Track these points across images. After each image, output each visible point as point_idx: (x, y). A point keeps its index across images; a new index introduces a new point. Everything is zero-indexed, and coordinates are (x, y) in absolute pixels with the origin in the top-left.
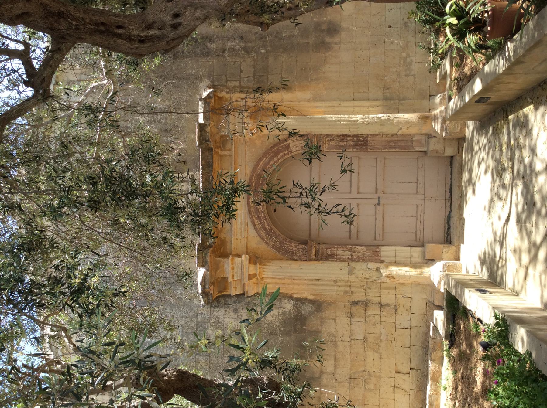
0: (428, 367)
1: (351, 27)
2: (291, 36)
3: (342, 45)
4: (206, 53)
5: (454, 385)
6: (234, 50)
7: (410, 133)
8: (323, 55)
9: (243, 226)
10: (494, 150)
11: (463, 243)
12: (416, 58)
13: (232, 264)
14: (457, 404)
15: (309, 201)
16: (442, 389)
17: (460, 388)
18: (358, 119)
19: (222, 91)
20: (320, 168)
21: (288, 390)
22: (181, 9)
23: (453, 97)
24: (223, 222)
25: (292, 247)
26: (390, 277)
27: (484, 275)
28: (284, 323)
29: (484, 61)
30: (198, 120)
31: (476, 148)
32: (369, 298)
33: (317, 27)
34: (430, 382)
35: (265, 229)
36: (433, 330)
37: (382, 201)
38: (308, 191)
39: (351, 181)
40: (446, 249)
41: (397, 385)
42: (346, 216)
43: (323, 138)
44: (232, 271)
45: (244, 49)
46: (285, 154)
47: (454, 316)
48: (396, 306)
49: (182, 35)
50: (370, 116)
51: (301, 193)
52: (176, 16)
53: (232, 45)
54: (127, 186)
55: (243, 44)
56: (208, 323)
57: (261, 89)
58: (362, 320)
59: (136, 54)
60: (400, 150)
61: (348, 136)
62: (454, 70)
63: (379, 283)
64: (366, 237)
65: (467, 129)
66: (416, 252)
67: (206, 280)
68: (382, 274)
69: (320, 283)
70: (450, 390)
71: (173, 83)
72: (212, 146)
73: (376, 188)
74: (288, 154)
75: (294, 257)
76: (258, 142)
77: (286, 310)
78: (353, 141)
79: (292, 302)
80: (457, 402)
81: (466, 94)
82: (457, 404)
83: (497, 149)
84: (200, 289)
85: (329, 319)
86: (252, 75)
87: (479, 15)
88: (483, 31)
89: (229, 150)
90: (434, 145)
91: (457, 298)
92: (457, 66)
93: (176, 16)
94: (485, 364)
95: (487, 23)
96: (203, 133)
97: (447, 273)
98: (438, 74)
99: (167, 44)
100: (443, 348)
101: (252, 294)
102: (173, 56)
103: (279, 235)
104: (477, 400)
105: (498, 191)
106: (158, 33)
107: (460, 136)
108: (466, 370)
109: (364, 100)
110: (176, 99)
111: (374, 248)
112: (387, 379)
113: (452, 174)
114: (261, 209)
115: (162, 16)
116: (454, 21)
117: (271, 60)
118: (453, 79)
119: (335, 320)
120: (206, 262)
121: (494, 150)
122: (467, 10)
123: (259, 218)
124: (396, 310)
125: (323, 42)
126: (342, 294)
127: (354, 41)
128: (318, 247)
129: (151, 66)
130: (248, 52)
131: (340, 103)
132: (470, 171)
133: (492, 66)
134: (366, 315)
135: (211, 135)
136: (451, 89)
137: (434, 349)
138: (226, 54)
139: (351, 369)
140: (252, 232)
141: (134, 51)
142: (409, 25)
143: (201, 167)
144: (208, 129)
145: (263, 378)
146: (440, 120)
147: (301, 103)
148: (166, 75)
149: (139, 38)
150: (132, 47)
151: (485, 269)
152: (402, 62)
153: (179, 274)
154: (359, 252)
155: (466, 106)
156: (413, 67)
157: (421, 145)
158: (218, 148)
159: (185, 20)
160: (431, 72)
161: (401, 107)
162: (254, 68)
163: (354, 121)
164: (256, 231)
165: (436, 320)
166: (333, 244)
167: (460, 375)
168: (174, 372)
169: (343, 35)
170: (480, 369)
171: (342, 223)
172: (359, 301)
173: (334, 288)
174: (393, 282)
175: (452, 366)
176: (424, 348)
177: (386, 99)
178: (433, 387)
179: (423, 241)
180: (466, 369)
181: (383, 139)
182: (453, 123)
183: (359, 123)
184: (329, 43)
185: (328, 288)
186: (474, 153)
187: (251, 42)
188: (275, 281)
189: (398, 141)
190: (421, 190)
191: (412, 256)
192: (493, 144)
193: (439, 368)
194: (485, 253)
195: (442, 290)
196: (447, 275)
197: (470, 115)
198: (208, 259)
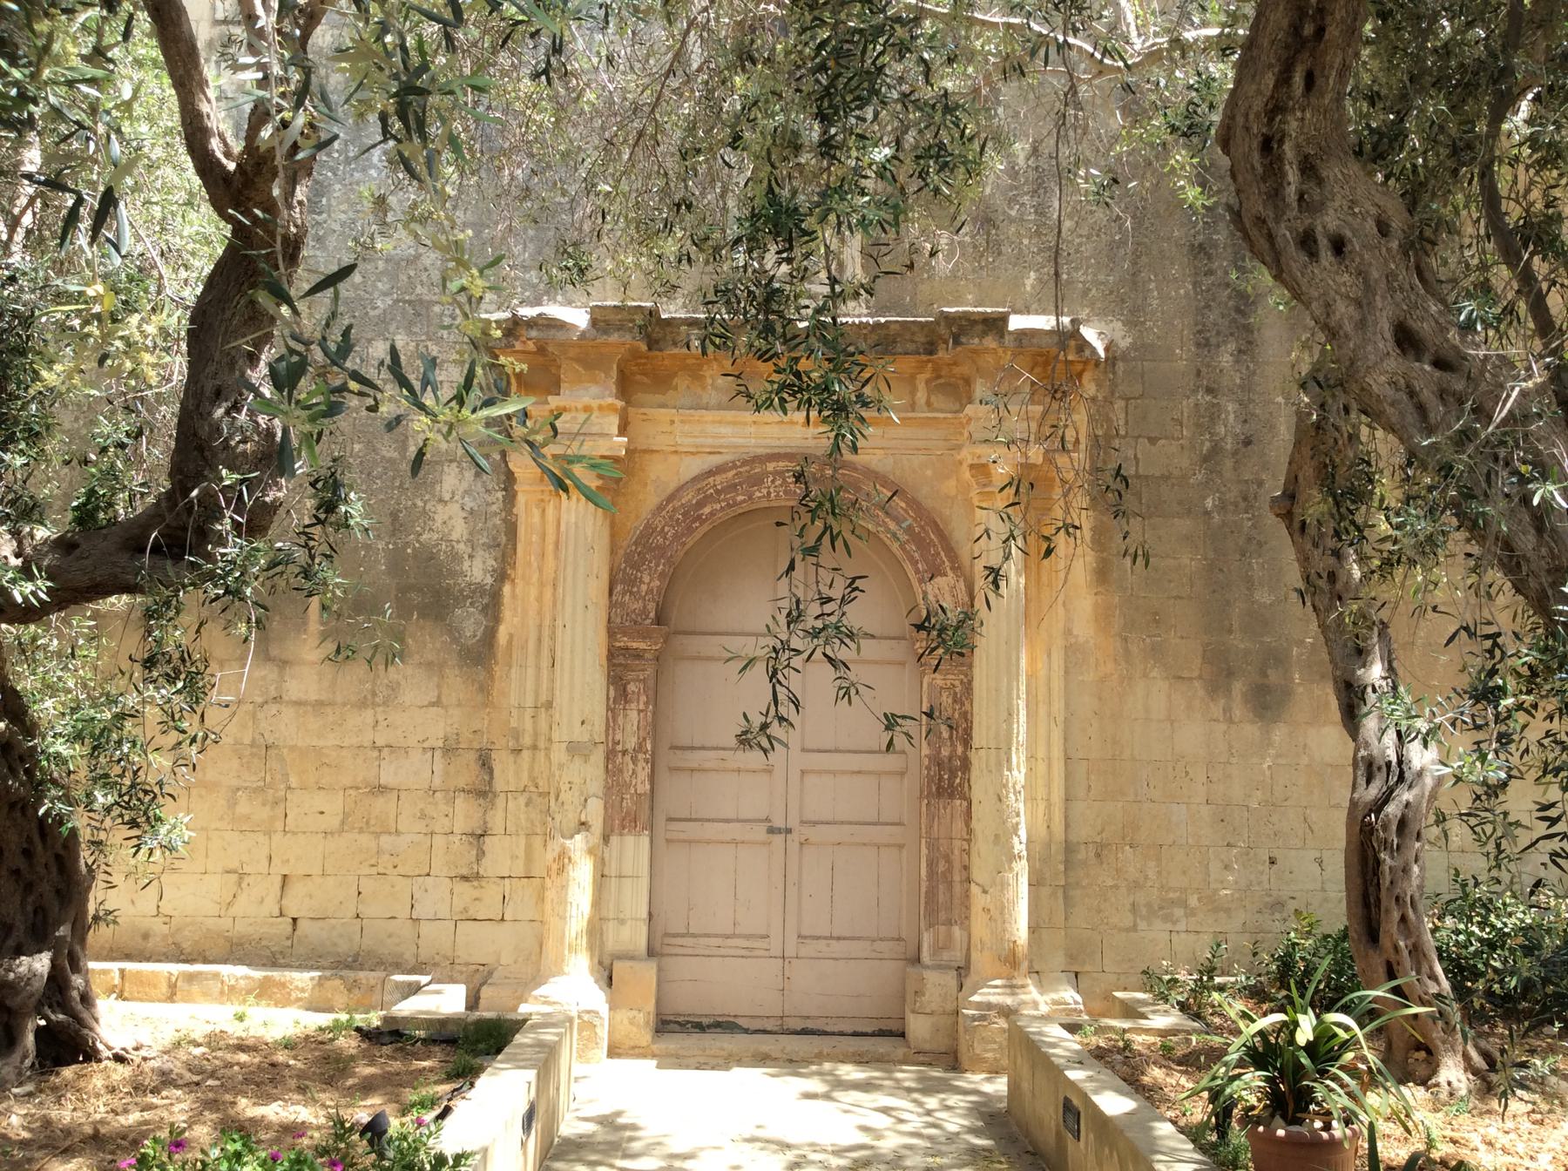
0: (302, 967)
1: (1272, 752)
2: (1250, 583)
3: (1223, 727)
4: (1207, 340)
5: (250, 1042)
6: (1214, 419)
7: (973, 918)
8: (1196, 674)
9: (710, 441)
10: (929, 1153)
11: (658, 1067)
12: (1183, 936)
13: (600, 408)
14: (198, 1051)
15: (810, 622)
16: (240, 1009)
17: (243, 1057)
18: (1015, 773)
19: (1099, 386)
20: (876, 662)
21: (250, 557)
22: (1358, 260)
23: (1077, 1038)
24: (738, 377)
25: (649, 582)
26: (563, 860)
27: (569, 1127)
28: (427, 557)
29: (1182, 1122)
30: (1016, 312)
31: (932, 1102)
32: (500, 801)
33: (1276, 658)
34: (258, 974)
35: (701, 504)
36: (410, 984)
37: (779, 839)
38: (833, 619)
39: (837, 751)
40: (641, 1017)
41: (247, 880)
42: (764, 726)
43: (961, 672)
44: (580, 406)
45: (1216, 450)
46: (914, 563)
47: (451, 1041)
48: (478, 876)
49: (1283, 260)
50: (1021, 806)
51: (830, 600)
52: (1338, 246)
53: (1228, 413)
54: (857, 93)
55: (1229, 445)
56: (427, 334)
57: (1122, 487)
58: (437, 782)
59: (1229, 128)
60: (923, 889)
61: (967, 742)
62: (1151, 1039)
63: (543, 830)
64: (675, 795)
65: (984, 1076)
66: (634, 936)
67: (553, 332)
68: (572, 837)
69: (545, 663)
70: (236, 1030)
71: (1123, 242)
72: (940, 354)
73: (815, 823)
74: (917, 571)
75: (619, 588)
76: (950, 486)
77: (466, 564)
78: (950, 759)
79: (489, 580)
80: (202, 1050)
81: (1090, 1073)
82: (198, 1051)
83: (930, 1160)
84: (527, 312)
85: (439, 686)
86: (1141, 471)
87: (1318, 1104)
88: (1272, 1116)
89: (928, 403)
90: (937, 984)
91: (506, 1050)
92: (1164, 1047)
93: (1338, 246)
94: (319, 1128)
95: (1295, 1128)
96: (980, 327)
97: (576, 1021)
98: (1140, 995)
99: (1258, 218)
100: (356, 1010)
101: (511, 465)
102: (1200, 245)
103: (684, 544)
104: (212, 1105)
105: (813, 1162)
106: (1291, 192)
107: (964, 1059)
108: (299, 1077)
109: (1067, 789)
110: (1077, 251)
111: (644, 816)
112: (265, 852)
113: (855, 1034)
114: (758, 494)
115: (1337, 204)
116: (1304, 1035)
117: (1184, 525)
118: (1127, 1036)
119: (437, 703)
120: (605, 332)
121: (929, 1153)
122: (1334, 1070)
123: (733, 487)
124: (465, 878)
125: (1230, 674)
126: (514, 724)
127: (1234, 760)
128: (647, 655)
129: (1180, 177)
130: (1206, 459)
131: (1060, 719)
132: (866, 1086)
133: (1172, 1144)
134: (452, 794)
135: (975, 352)
136: (1100, 1030)
137: (352, 986)
138: (1203, 398)
139: (293, 748)
140: (692, 467)
141: (1240, 120)
142: (1277, 916)
143: (883, 320)
144: (990, 342)
145: (280, 490)
146: (1009, 1001)
147: (1061, 610)
148: (1147, 224)
149: (1277, 137)
150: (1252, 117)
151: (590, 1128)
152: (1171, 895)
153: (583, 248)
154: (634, 772)
155: (1054, 1072)
156: (1158, 924)
157: (937, 949)
158: (934, 370)
159: (1327, 273)
160: (1145, 977)
161: (1045, 891)
162: (1162, 477)
163: (1009, 760)
164: (695, 479)
165: (438, 992)
166: (655, 698)
167: (281, 1057)
168: (296, 226)
169: (1251, 730)
170: (300, 1112)
171: (745, 715)
172: (491, 772)
173: (529, 702)
174: (549, 869)
175: (307, 1036)
176: (356, 957)
177: (1069, 848)
178: (242, 982)
179: (663, 955)
180: (301, 1075)
181: (957, 844)
182: (1002, 1039)
183: (1002, 775)
184: (1229, 691)
185: (530, 685)
186: (916, 1096)
187: (1235, 469)
188: (551, 530)
189: (950, 884)
190: (810, 949)
191: (622, 922)
192: (944, 1148)
193: (298, 1000)
194: (634, 1127)
195: (524, 1009)
196: (571, 1020)
197: (1025, 1086)
198: (614, 338)
